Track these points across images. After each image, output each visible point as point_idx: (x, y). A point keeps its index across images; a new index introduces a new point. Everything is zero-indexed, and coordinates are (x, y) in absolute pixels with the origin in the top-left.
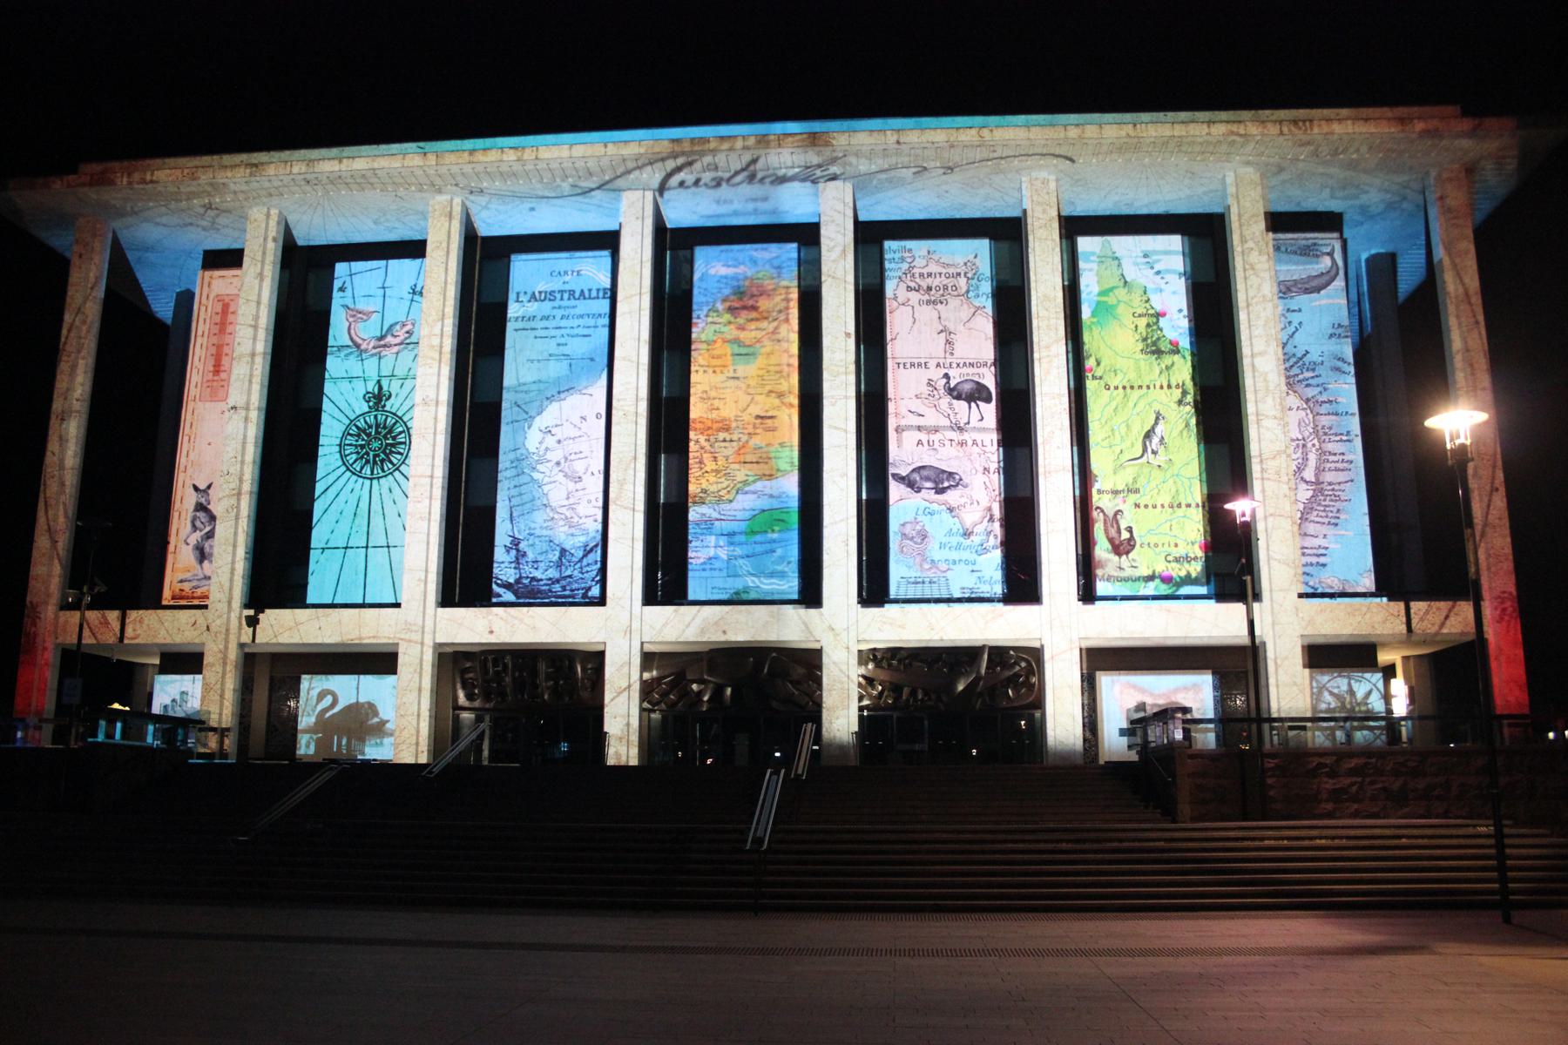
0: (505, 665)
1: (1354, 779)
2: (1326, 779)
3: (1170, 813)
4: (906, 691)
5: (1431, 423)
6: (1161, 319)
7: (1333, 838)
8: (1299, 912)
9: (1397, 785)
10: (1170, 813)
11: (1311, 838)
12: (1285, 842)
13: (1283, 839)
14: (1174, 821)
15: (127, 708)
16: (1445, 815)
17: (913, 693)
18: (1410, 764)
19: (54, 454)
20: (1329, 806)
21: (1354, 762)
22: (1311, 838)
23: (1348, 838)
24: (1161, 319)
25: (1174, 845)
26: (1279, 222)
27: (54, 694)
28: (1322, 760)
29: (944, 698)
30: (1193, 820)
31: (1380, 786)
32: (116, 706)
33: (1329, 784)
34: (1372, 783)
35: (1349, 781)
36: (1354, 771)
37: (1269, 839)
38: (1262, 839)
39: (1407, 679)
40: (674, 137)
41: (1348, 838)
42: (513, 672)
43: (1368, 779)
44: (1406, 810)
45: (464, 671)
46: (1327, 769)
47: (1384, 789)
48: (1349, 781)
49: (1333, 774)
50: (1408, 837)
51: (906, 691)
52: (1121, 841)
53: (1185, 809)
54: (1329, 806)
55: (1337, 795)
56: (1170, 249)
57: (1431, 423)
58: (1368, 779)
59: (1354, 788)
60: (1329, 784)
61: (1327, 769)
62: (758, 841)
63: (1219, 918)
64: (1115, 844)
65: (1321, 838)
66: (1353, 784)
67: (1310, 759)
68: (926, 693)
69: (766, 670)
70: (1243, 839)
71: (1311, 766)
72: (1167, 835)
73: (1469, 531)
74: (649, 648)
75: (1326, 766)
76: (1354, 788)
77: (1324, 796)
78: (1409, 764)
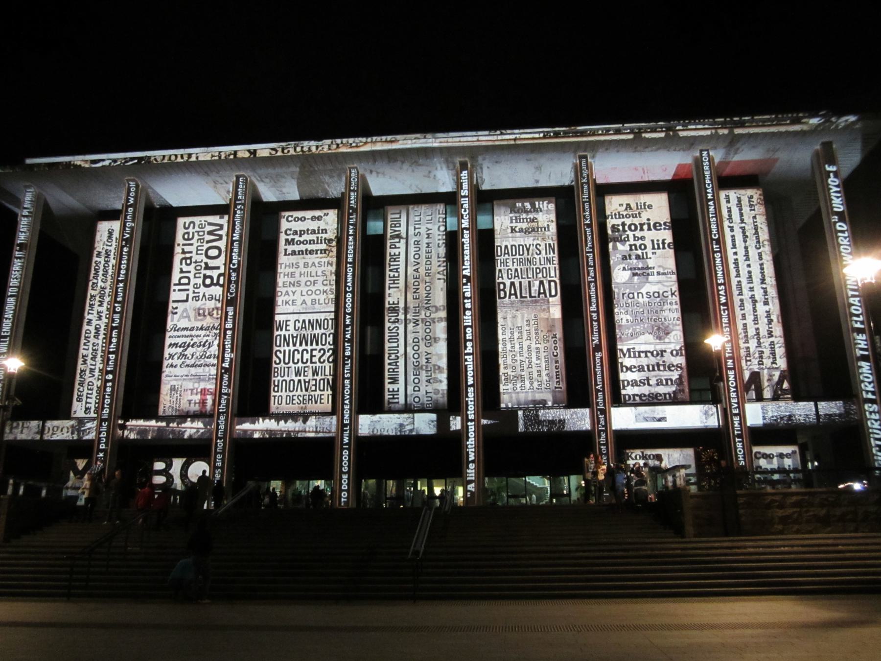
1: (795, 510)
2: (778, 510)
3: (679, 531)
5: (706, 341)
6: (187, 319)
7: (792, 546)
8: (753, 597)
9: (823, 512)
10: (679, 531)
11: (778, 547)
12: (761, 549)
13: (759, 547)
14: (683, 537)
15: (841, 486)
16: (856, 531)
19: (426, 386)
20: (780, 527)
21: (794, 499)
22: (778, 547)
23: (802, 546)
24: (187, 319)
25: (663, 552)
28: (774, 498)
30: (695, 536)
31: (811, 513)
32: (857, 486)
33: (780, 513)
34: (807, 512)
36: (795, 505)
37: (750, 547)
38: (745, 547)
41: (802, 546)
44: (829, 529)
46: (777, 503)
49: (782, 506)
50: (843, 545)
52: (652, 550)
53: (689, 529)
54: (780, 527)
55: (784, 520)
56: (185, 299)
57: (706, 341)
58: (804, 509)
59: (796, 515)
60: (780, 513)
61: (777, 503)
62: (416, 553)
63: (726, 601)
64: (649, 552)
65: (784, 546)
66: (794, 513)
67: (767, 497)
70: (772, 547)
71: (766, 502)
72: (682, 546)
75: (776, 501)
76: (796, 515)
78: (830, 499)
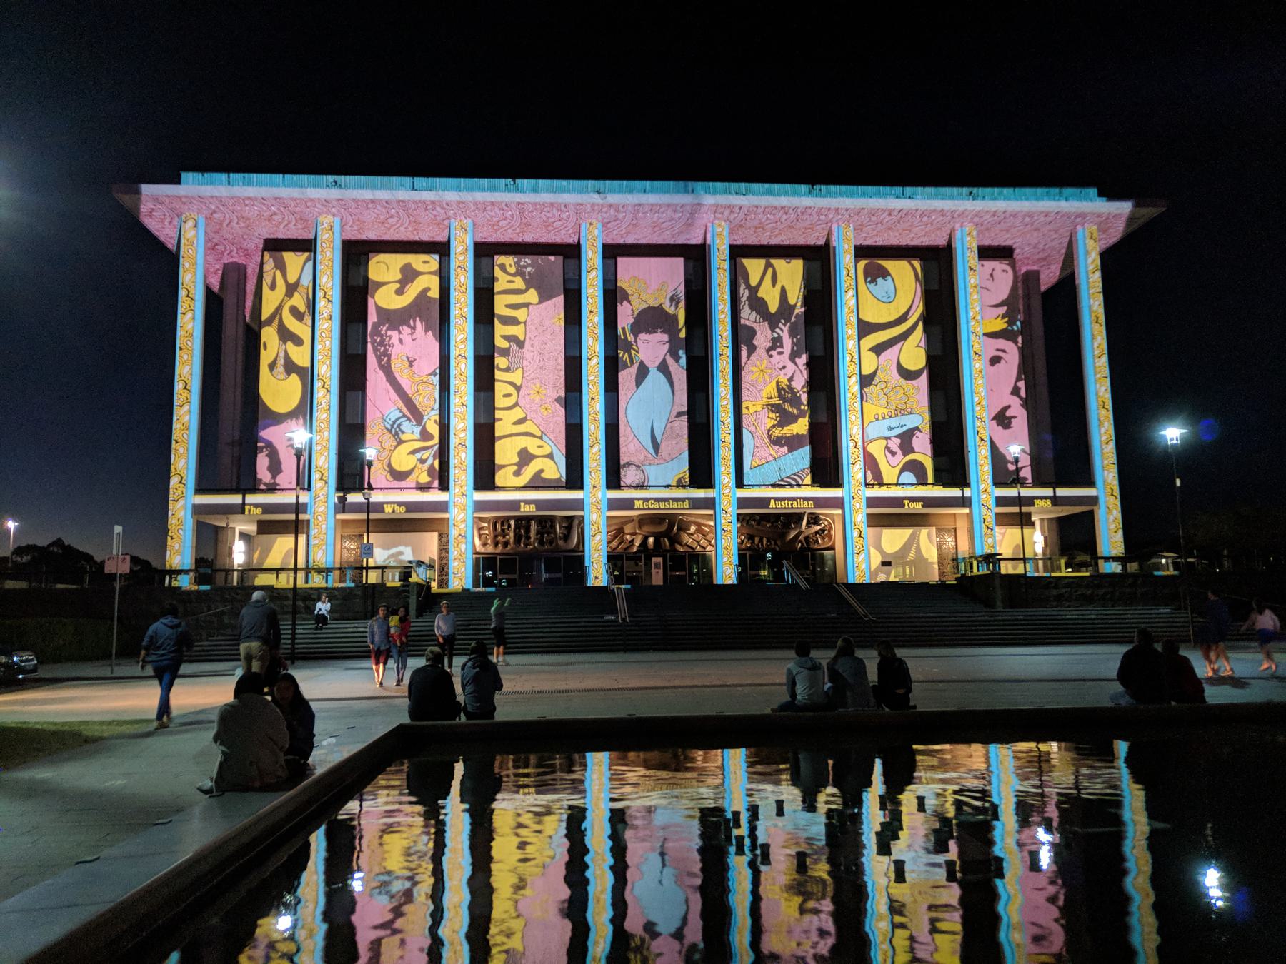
0: (509, 526)
4: (757, 540)
16: (1113, 606)
17: (761, 541)
18: (1095, 582)
26: (862, 252)
27: (975, 520)
29: (779, 543)
31: (1079, 593)
33: (1055, 592)
35: (1064, 590)
39: (1043, 533)
40: (512, 284)
42: (515, 530)
43: (1073, 590)
45: (480, 529)
47: (1082, 595)
48: (1064, 590)
51: (757, 540)
58: (1073, 590)
60: (1055, 592)
68: (768, 540)
69: (59, 586)
73: (772, 504)
74: (931, 846)
77: (1052, 599)
